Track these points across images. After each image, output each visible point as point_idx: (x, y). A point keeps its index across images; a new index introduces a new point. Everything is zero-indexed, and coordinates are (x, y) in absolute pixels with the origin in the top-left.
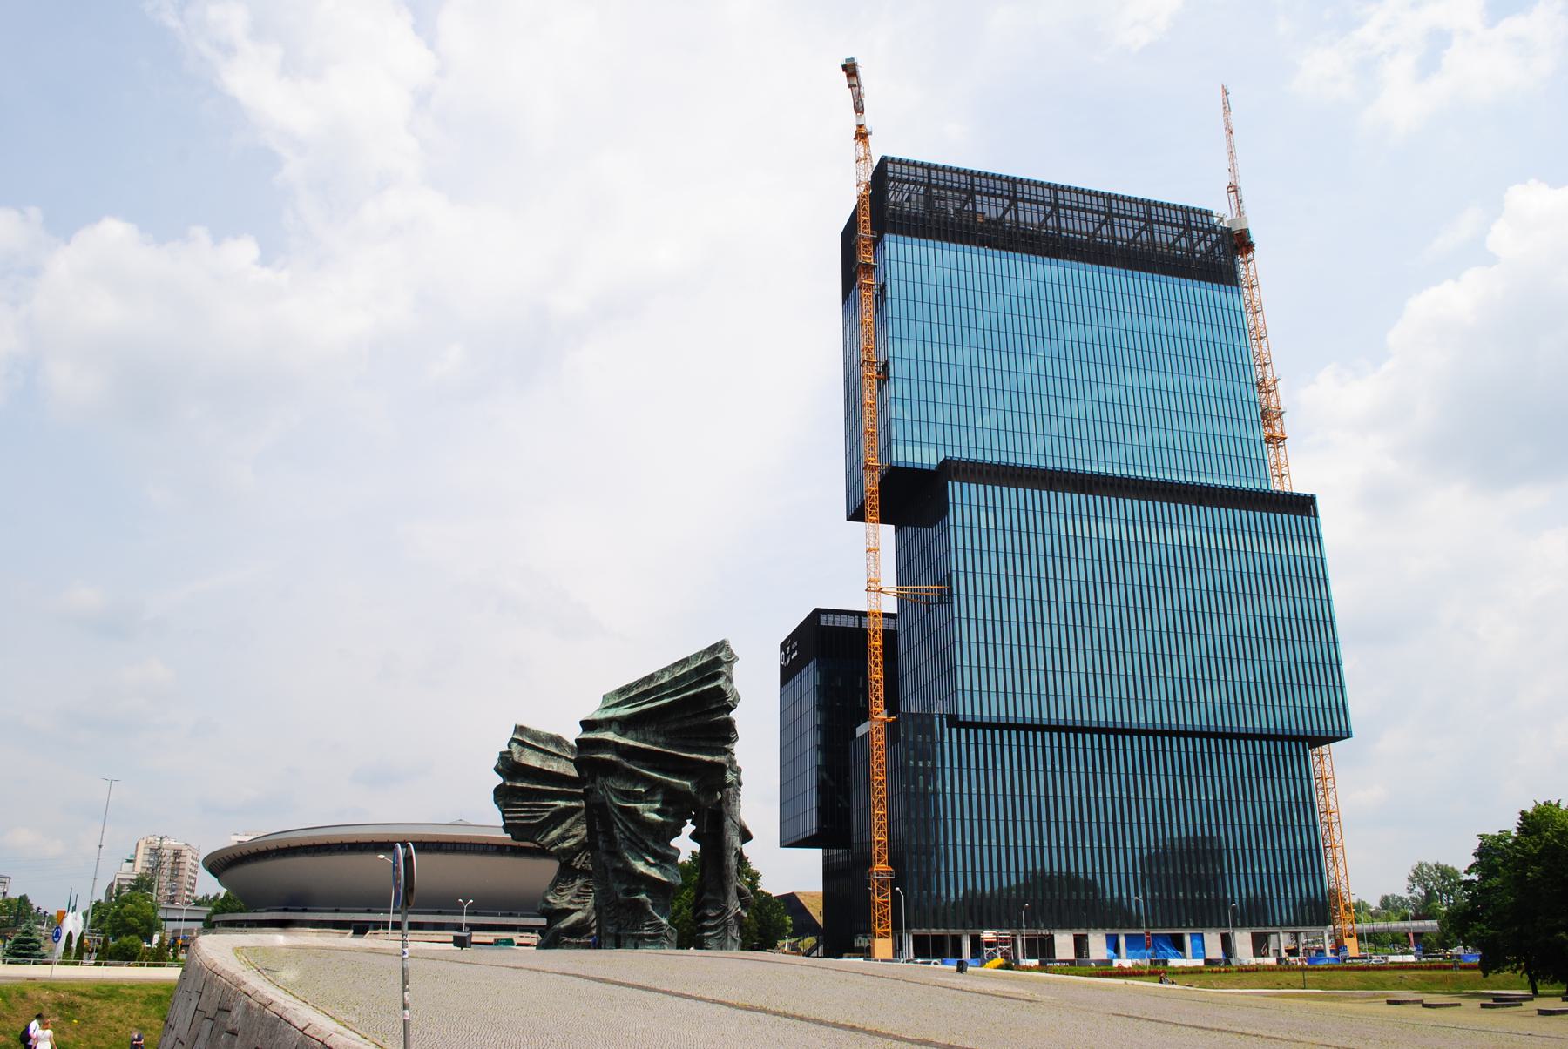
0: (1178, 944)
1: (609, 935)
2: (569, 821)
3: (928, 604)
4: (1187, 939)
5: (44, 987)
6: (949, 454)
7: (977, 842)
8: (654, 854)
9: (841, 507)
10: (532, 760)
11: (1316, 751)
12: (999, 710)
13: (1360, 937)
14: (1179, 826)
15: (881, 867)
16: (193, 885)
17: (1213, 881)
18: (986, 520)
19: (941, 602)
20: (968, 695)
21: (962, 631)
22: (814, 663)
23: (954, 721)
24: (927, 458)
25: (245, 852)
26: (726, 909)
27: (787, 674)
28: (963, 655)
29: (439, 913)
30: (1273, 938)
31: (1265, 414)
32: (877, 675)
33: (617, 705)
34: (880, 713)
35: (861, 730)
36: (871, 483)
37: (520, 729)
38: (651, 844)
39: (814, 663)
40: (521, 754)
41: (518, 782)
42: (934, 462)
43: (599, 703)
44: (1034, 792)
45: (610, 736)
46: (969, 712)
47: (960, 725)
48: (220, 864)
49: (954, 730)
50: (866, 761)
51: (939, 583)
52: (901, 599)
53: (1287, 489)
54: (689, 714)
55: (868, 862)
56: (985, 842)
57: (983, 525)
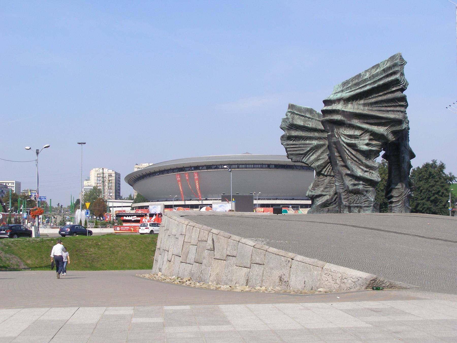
2: (320, 151)
8: (367, 166)
10: (299, 122)
33: (342, 91)
37: (291, 106)
41: (293, 132)
45: (339, 107)
48: (135, 179)
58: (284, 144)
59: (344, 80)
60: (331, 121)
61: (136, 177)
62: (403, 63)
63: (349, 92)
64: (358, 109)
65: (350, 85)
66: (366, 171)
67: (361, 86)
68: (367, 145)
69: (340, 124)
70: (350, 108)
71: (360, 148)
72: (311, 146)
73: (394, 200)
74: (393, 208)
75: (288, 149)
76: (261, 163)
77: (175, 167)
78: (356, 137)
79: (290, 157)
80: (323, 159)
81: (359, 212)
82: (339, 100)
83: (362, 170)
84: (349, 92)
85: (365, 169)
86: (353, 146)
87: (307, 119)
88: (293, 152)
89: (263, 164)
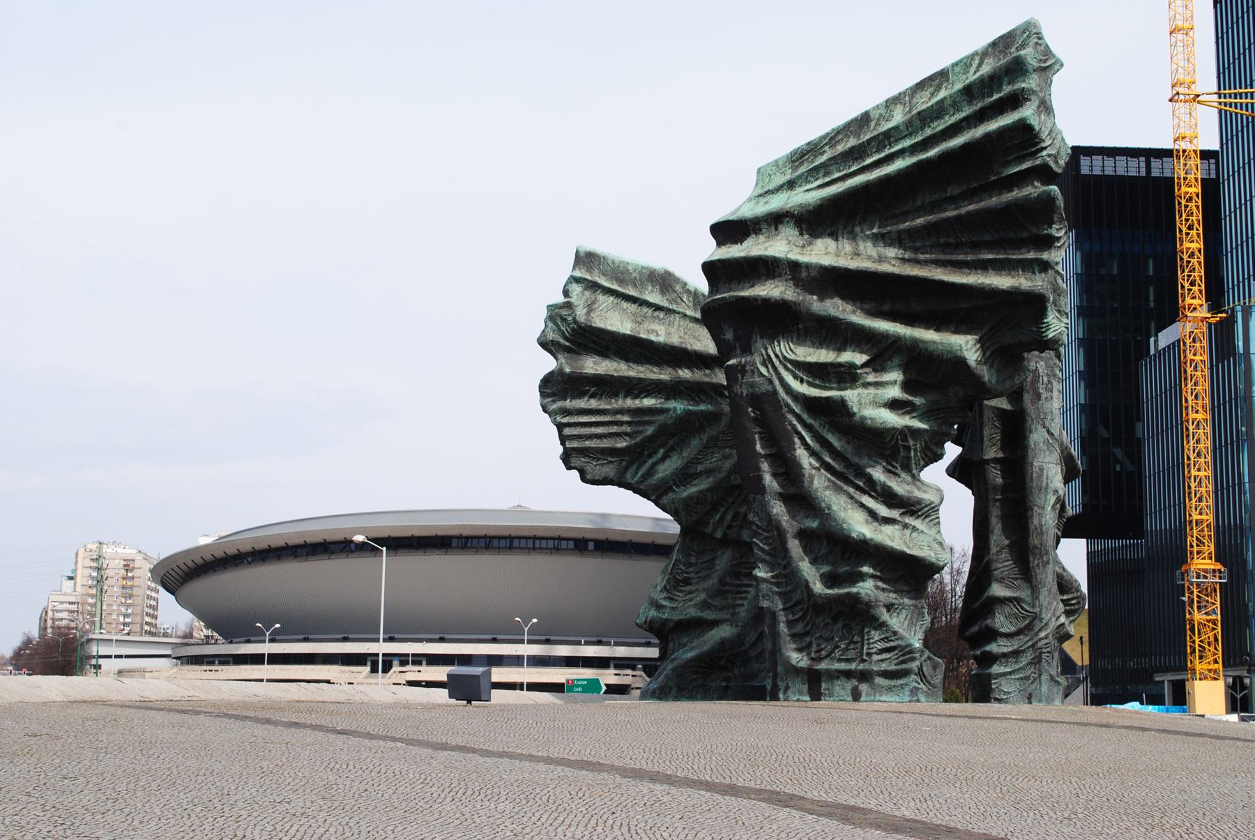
1: (797, 671)
2: (695, 442)
8: (890, 498)
10: (615, 319)
15: (1203, 564)
16: (155, 608)
26: (1036, 617)
29: (494, 641)
32: (1191, 244)
33: (791, 185)
35: (1165, 338)
37: (586, 259)
38: (878, 474)
40: (590, 308)
41: (601, 374)
43: (748, 186)
45: (780, 245)
48: (181, 575)
52: (1224, 118)
54: (953, 191)
55: (1178, 555)
58: (554, 406)
60: (740, 302)
61: (184, 567)
62: (1048, 66)
63: (820, 187)
64: (857, 254)
65: (824, 158)
66: (888, 521)
67: (869, 161)
68: (894, 405)
69: (782, 321)
70: (824, 253)
71: (864, 418)
72: (661, 418)
73: (1001, 621)
74: (994, 684)
75: (567, 431)
76: (555, 534)
77: (300, 541)
78: (847, 375)
79: (576, 461)
80: (709, 472)
81: (856, 696)
82: (775, 220)
83: (872, 514)
84: (820, 187)
85: (883, 511)
86: (832, 414)
87: (649, 311)
88: (588, 443)
89: (560, 539)
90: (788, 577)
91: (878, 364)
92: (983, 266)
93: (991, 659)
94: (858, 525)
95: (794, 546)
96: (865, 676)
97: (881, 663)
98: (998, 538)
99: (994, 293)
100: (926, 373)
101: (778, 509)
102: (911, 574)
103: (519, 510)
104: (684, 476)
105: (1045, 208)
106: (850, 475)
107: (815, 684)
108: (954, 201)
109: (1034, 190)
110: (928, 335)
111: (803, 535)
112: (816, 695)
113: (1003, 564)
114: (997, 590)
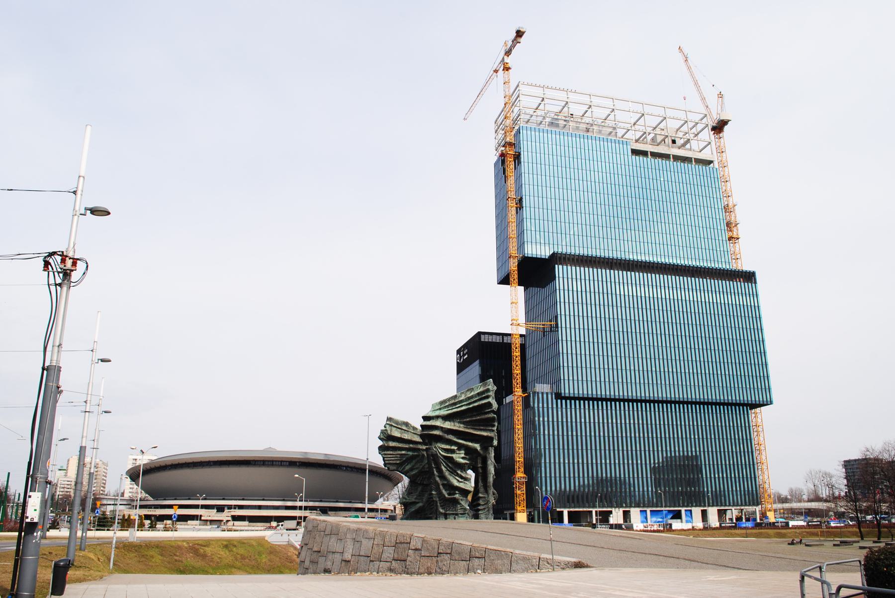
0: (677, 516)
3: (544, 332)
4: (683, 513)
5: (183, 541)
6: (556, 250)
7: (571, 461)
8: (462, 477)
9: (494, 277)
10: (396, 433)
11: (753, 411)
12: (584, 391)
13: (775, 511)
14: (679, 449)
17: (696, 481)
18: (576, 286)
19: (551, 331)
20: (566, 382)
21: (563, 347)
22: (477, 362)
23: (558, 396)
24: (544, 252)
25: (153, 466)
27: (461, 367)
28: (564, 361)
30: (729, 513)
31: (728, 224)
32: (517, 371)
34: (518, 391)
35: (508, 399)
36: (513, 265)
37: (389, 419)
38: (459, 472)
39: (477, 362)
41: (389, 441)
42: (548, 254)
43: (430, 408)
44: (602, 434)
45: (438, 423)
46: (567, 391)
47: (562, 398)
49: (559, 401)
50: (512, 415)
51: (551, 321)
53: (740, 268)
55: (513, 472)
56: (576, 461)
57: (575, 289)
59: (442, 399)
60: (428, 434)
68: (463, 458)
70: (448, 425)
73: (481, 502)
78: (453, 451)
82: (437, 417)
86: (451, 459)
90: (440, 493)
91: (459, 449)
92: (481, 430)
93: (479, 510)
94: (456, 483)
95: (441, 487)
96: (457, 514)
97: (460, 511)
98: (480, 484)
99: (483, 436)
100: (469, 451)
101: (438, 479)
102: (465, 493)
103: (269, 450)
104: (411, 469)
105: (493, 419)
106: (453, 473)
107: (446, 516)
108: (475, 416)
109: (492, 415)
110: (470, 444)
111: (443, 485)
112: (446, 518)
113: (482, 489)
114: (480, 495)
